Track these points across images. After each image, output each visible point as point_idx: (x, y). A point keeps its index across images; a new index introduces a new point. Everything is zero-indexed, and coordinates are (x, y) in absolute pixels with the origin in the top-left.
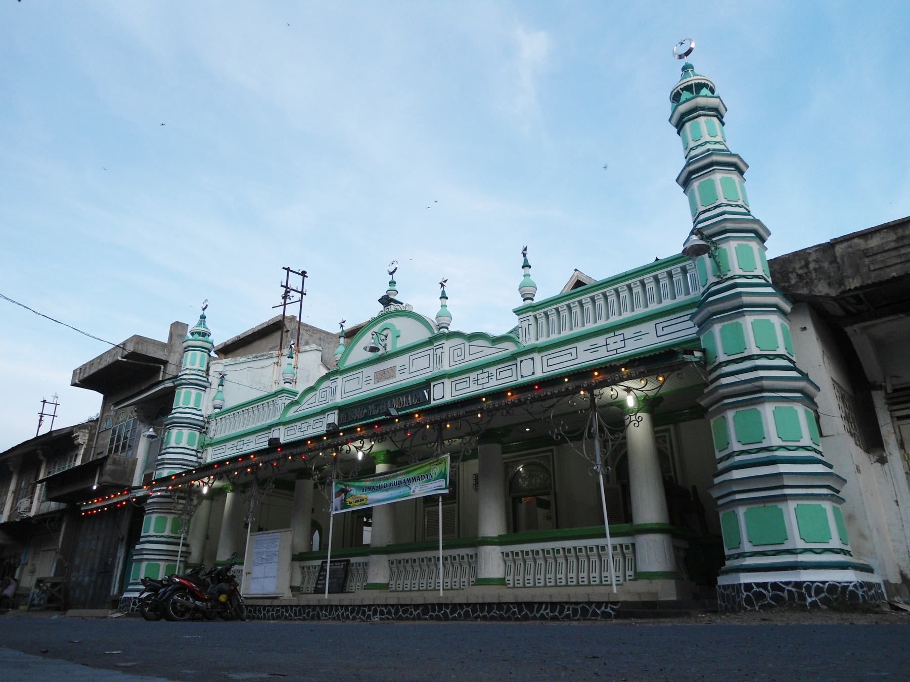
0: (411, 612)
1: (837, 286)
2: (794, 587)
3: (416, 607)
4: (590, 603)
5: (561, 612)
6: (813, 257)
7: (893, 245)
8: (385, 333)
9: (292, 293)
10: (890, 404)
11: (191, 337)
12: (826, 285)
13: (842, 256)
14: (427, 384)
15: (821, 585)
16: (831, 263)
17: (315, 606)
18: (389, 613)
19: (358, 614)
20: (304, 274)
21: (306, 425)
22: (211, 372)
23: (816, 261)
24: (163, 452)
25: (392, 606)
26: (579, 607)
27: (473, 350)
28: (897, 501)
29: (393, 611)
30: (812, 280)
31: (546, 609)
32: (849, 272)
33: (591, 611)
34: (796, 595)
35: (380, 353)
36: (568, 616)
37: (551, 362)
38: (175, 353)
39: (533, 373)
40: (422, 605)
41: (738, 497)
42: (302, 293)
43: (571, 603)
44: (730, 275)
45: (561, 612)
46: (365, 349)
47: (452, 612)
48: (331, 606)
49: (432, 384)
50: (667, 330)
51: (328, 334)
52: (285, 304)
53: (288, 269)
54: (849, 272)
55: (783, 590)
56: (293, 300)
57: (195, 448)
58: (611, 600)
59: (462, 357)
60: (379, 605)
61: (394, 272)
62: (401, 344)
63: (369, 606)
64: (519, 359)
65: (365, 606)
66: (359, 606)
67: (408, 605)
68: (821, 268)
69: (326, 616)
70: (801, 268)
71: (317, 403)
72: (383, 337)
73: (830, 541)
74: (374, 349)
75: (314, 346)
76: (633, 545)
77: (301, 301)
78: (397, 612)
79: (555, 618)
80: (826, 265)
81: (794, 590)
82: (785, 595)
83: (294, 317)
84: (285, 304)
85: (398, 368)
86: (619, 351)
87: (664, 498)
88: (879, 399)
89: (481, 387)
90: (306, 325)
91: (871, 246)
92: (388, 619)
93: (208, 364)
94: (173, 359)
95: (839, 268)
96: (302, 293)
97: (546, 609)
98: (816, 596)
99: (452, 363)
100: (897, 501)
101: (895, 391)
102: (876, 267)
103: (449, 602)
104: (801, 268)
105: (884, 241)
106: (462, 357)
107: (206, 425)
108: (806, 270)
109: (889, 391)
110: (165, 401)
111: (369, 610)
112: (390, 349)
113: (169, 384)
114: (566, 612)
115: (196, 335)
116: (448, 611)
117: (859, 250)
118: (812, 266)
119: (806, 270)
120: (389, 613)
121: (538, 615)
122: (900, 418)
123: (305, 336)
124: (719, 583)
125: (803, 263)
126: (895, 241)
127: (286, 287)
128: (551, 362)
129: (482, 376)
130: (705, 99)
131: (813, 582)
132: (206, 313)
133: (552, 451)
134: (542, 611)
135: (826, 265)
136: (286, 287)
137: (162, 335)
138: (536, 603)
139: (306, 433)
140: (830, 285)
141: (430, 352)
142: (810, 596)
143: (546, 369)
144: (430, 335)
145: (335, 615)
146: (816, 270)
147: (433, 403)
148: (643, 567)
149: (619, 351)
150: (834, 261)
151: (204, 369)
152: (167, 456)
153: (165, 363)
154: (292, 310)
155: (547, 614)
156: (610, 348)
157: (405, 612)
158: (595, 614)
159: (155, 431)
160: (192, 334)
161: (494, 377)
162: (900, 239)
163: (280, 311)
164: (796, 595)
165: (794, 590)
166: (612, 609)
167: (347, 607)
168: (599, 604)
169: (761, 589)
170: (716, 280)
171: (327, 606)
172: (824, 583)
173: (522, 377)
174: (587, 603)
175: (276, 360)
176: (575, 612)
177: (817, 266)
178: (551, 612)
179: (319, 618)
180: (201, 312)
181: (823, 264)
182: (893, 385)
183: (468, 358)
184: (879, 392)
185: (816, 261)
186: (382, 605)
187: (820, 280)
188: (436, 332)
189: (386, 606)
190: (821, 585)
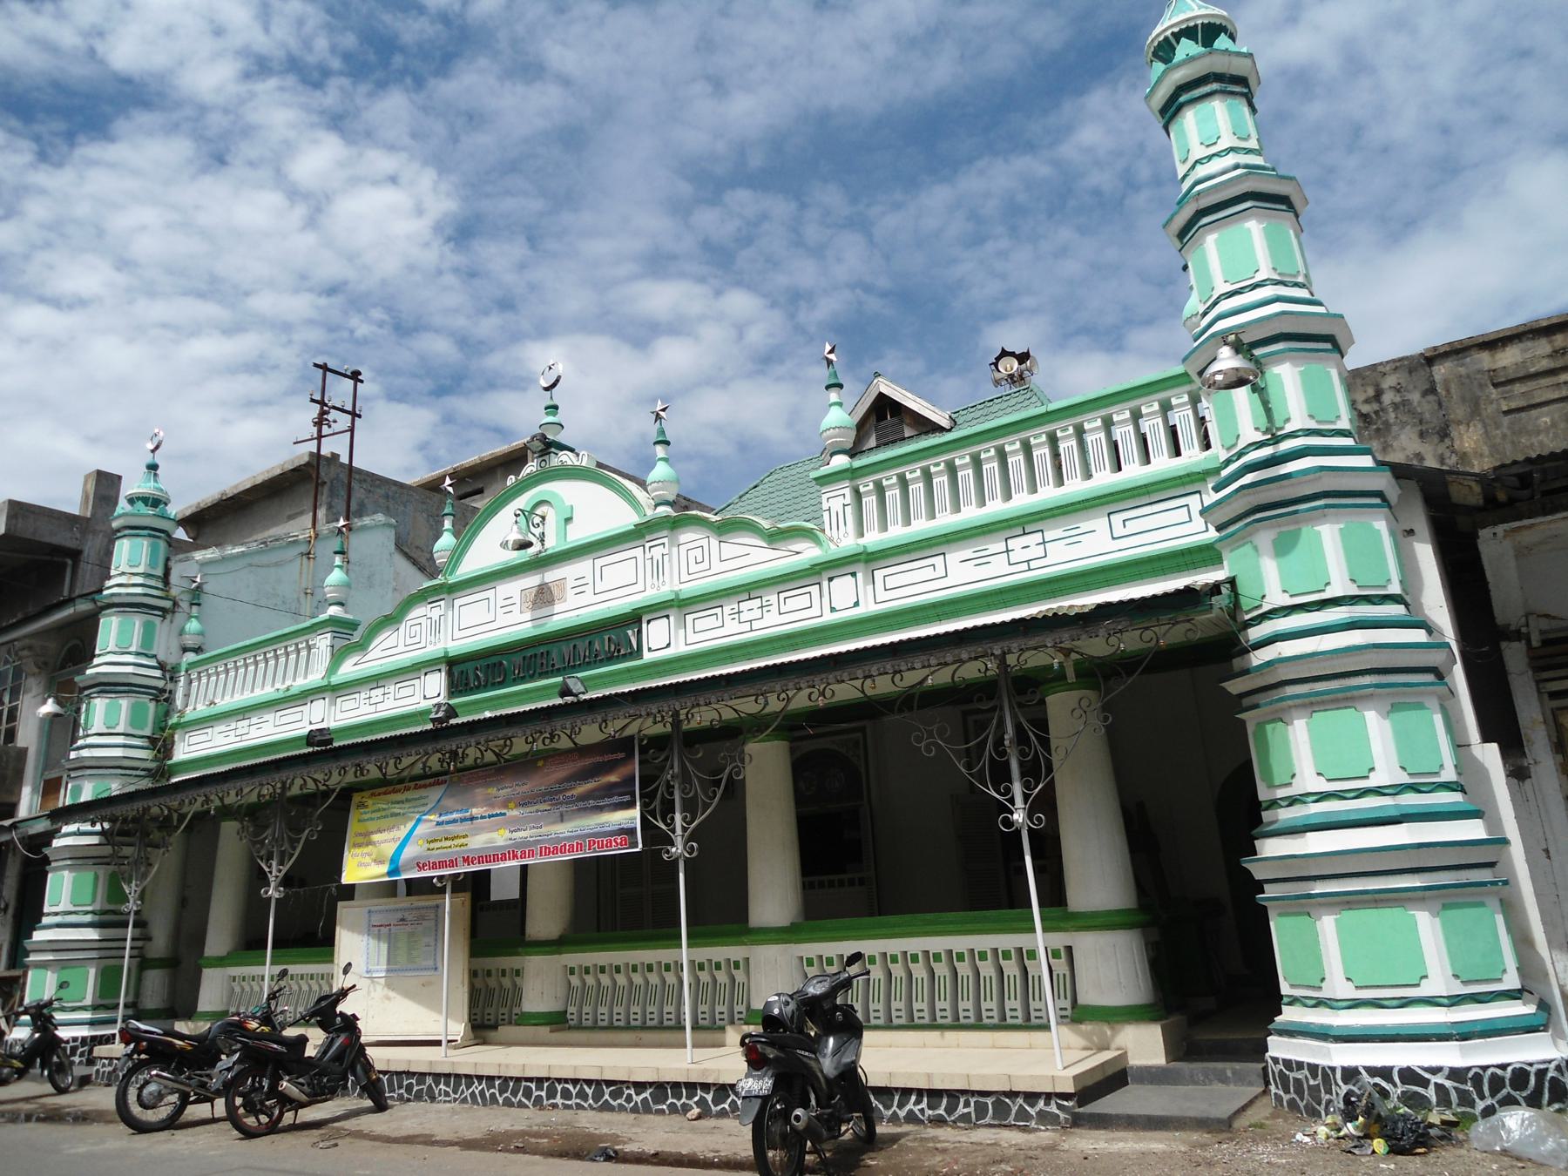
0: (630, 1096)
1: (1436, 439)
2: (1448, 1078)
3: (640, 1086)
4: (1013, 1094)
5: (950, 1110)
6: (1390, 381)
7: (1545, 364)
8: (538, 511)
9: (333, 415)
10: (1537, 669)
11: (128, 508)
12: (1415, 436)
13: (1446, 382)
14: (634, 619)
15: (1499, 1072)
16: (1425, 394)
17: (423, 1075)
18: (582, 1095)
19: (515, 1093)
20: (355, 376)
21: (381, 691)
22: (173, 579)
23: (1397, 389)
24: (80, 742)
25: (589, 1082)
26: (989, 1101)
27: (729, 549)
28: (1547, 851)
29: (590, 1092)
30: (1387, 425)
31: (918, 1102)
32: (1459, 412)
33: (1014, 1109)
34: (1454, 1096)
35: (531, 551)
36: (965, 1118)
37: (891, 582)
38: (95, 532)
39: (856, 604)
40: (651, 1084)
41: (1319, 888)
42: (354, 415)
43: (973, 1093)
44: (1289, 428)
45: (950, 1110)
46: (504, 545)
47: (716, 1102)
48: (458, 1076)
49: (645, 619)
50: (1133, 527)
51: (402, 486)
52: (320, 437)
53: (325, 368)
54: (1459, 412)
55: (1425, 1083)
56: (336, 427)
57: (141, 570)
58: (1058, 1090)
59: (705, 565)
60: (559, 1080)
61: (554, 385)
62: (579, 534)
63: (540, 1081)
64: (826, 575)
65: (530, 1080)
66: (518, 1080)
67: (623, 1082)
68: (1405, 403)
69: (446, 1094)
70: (1367, 401)
71: (401, 648)
72: (537, 520)
73: (1505, 977)
74: (524, 545)
75: (380, 517)
76: (1069, 949)
77: (352, 430)
78: (597, 1097)
79: (939, 1122)
80: (1415, 397)
81: (1448, 1084)
82: (1431, 1093)
83: (335, 456)
84: (320, 437)
85: (570, 583)
86: (1033, 564)
87: (1128, 856)
88: (1514, 656)
89: (747, 627)
90: (360, 471)
91: (1500, 364)
92: (579, 1107)
93: (168, 559)
94: (91, 548)
95: (1440, 405)
96: (354, 415)
97: (918, 1102)
98: (1493, 1096)
99: (685, 577)
100: (1547, 851)
101: (1546, 643)
102: (1513, 405)
103: (710, 1081)
104: (1367, 401)
105: (1528, 355)
106: (705, 565)
107: (170, 686)
108: (1376, 406)
109: (1535, 644)
110: (78, 643)
111: (540, 1088)
112: (553, 544)
113: (83, 606)
114: (961, 1110)
115: (140, 504)
116: (709, 1097)
117: (1479, 371)
118: (1388, 398)
119: (1376, 406)
120: (582, 1095)
121: (902, 1114)
122: (1554, 695)
123: (358, 493)
124: (1272, 1052)
125: (1371, 392)
126: (1550, 356)
127: (322, 403)
128: (891, 582)
129: (750, 608)
130: (1226, 59)
131: (1485, 1068)
132: (159, 458)
133: (863, 730)
134: (910, 1106)
135: (1415, 397)
136: (322, 403)
137: (69, 498)
138: (897, 1089)
139: (380, 707)
140: (1422, 435)
141: (638, 552)
142: (1482, 1098)
143: (938, 560)
144: (636, 519)
145: (467, 1093)
146: (1395, 406)
147: (648, 656)
148: (1088, 997)
149: (756, 625)
150: (1432, 390)
151: (159, 572)
152: (85, 753)
153: (76, 555)
154: (334, 446)
155: (922, 1111)
156: (1014, 557)
157: (616, 1095)
158: (1023, 1115)
159: (58, 702)
160: (131, 501)
161: (774, 608)
162: (1556, 353)
163: (312, 447)
164: (1454, 1096)
165: (1448, 1084)
166: (1059, 1107)
167: (491, 1079)
168: (1031, 1097)
169: (1378, 1080)
170: (1259, 437)
171: (448, 1076)
172: (1503, 1067)
173: (833, 610)
174: (1005, 1094)
175: (304, 549)
176: (981, 1110)
177: (1398, 399)
178: (930, 1107)
179: (433, 1099)
180: (149, 459)
181: (1409, 396)
182: (1542, 632)
183: (717, 567)
184: (1516, 645)
185: (1397, 389)
186: (566, 1081)
187: (1403, 425)
188: (650, 513)
189: (575, 1082)
190: (1499, 1072)
